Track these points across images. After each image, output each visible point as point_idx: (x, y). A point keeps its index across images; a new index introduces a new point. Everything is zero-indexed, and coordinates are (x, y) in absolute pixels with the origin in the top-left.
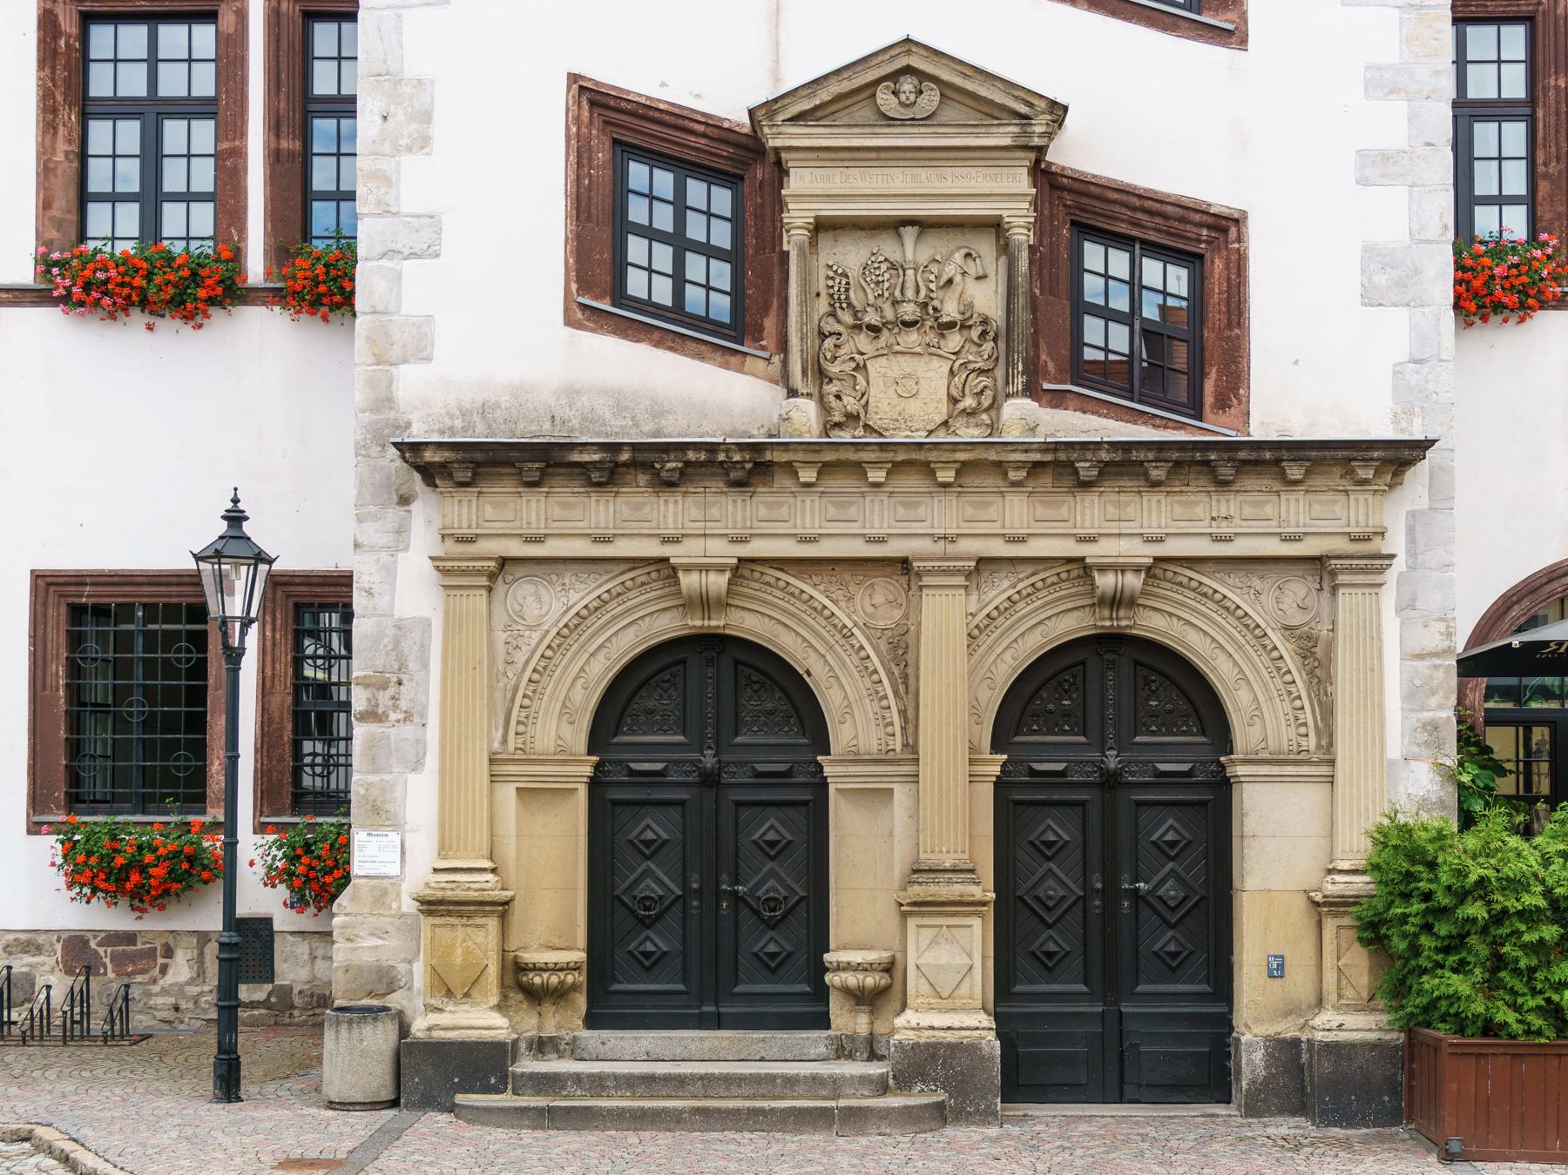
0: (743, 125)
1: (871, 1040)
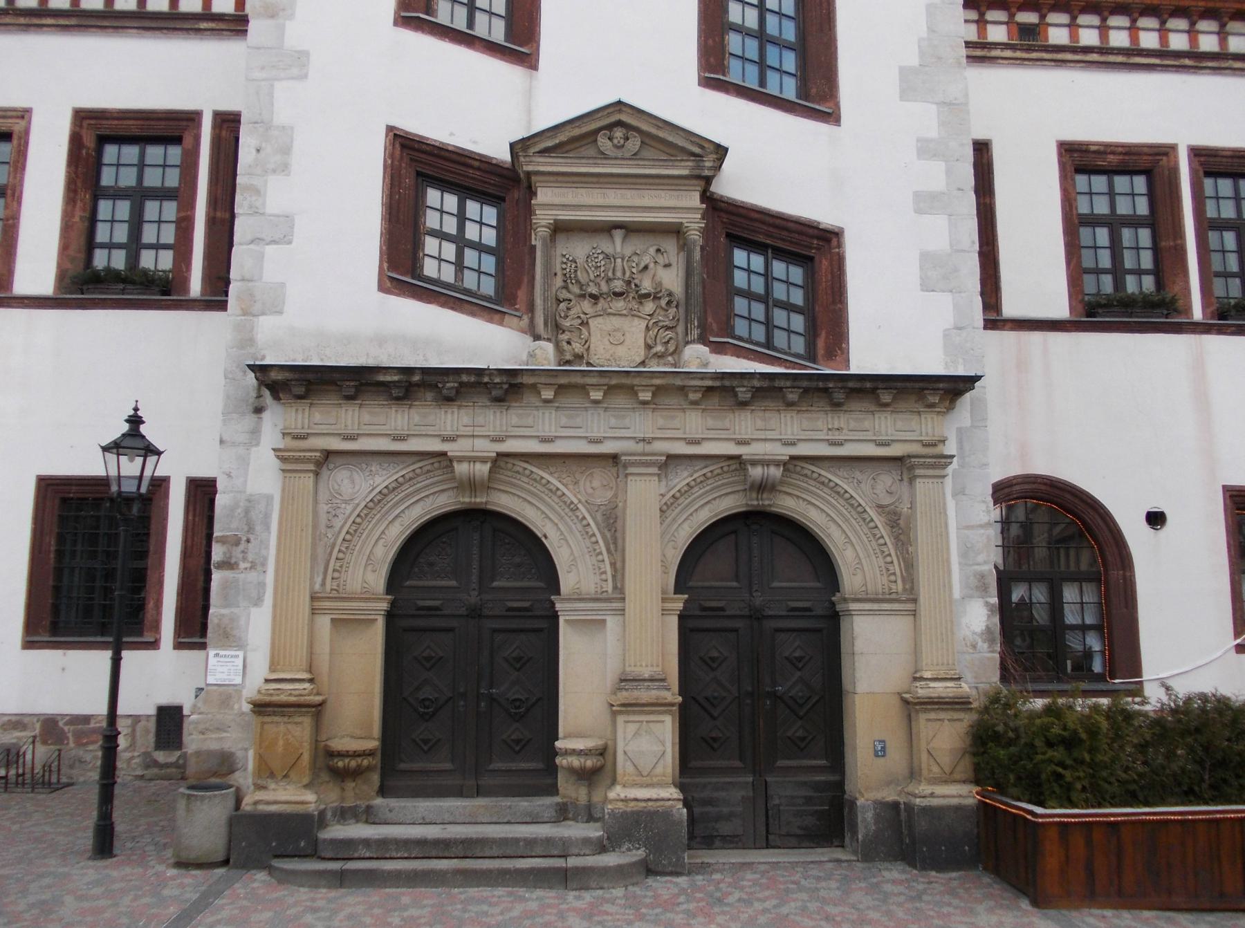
0: (505, 162)
1: (589, 807)
